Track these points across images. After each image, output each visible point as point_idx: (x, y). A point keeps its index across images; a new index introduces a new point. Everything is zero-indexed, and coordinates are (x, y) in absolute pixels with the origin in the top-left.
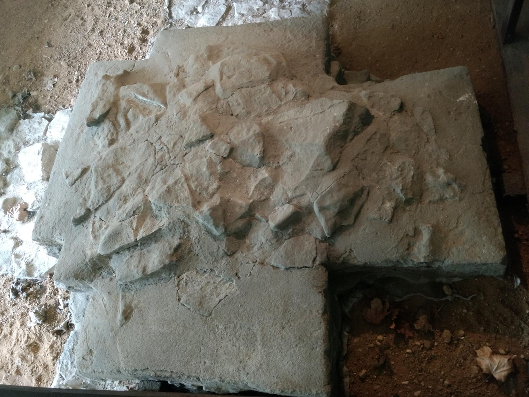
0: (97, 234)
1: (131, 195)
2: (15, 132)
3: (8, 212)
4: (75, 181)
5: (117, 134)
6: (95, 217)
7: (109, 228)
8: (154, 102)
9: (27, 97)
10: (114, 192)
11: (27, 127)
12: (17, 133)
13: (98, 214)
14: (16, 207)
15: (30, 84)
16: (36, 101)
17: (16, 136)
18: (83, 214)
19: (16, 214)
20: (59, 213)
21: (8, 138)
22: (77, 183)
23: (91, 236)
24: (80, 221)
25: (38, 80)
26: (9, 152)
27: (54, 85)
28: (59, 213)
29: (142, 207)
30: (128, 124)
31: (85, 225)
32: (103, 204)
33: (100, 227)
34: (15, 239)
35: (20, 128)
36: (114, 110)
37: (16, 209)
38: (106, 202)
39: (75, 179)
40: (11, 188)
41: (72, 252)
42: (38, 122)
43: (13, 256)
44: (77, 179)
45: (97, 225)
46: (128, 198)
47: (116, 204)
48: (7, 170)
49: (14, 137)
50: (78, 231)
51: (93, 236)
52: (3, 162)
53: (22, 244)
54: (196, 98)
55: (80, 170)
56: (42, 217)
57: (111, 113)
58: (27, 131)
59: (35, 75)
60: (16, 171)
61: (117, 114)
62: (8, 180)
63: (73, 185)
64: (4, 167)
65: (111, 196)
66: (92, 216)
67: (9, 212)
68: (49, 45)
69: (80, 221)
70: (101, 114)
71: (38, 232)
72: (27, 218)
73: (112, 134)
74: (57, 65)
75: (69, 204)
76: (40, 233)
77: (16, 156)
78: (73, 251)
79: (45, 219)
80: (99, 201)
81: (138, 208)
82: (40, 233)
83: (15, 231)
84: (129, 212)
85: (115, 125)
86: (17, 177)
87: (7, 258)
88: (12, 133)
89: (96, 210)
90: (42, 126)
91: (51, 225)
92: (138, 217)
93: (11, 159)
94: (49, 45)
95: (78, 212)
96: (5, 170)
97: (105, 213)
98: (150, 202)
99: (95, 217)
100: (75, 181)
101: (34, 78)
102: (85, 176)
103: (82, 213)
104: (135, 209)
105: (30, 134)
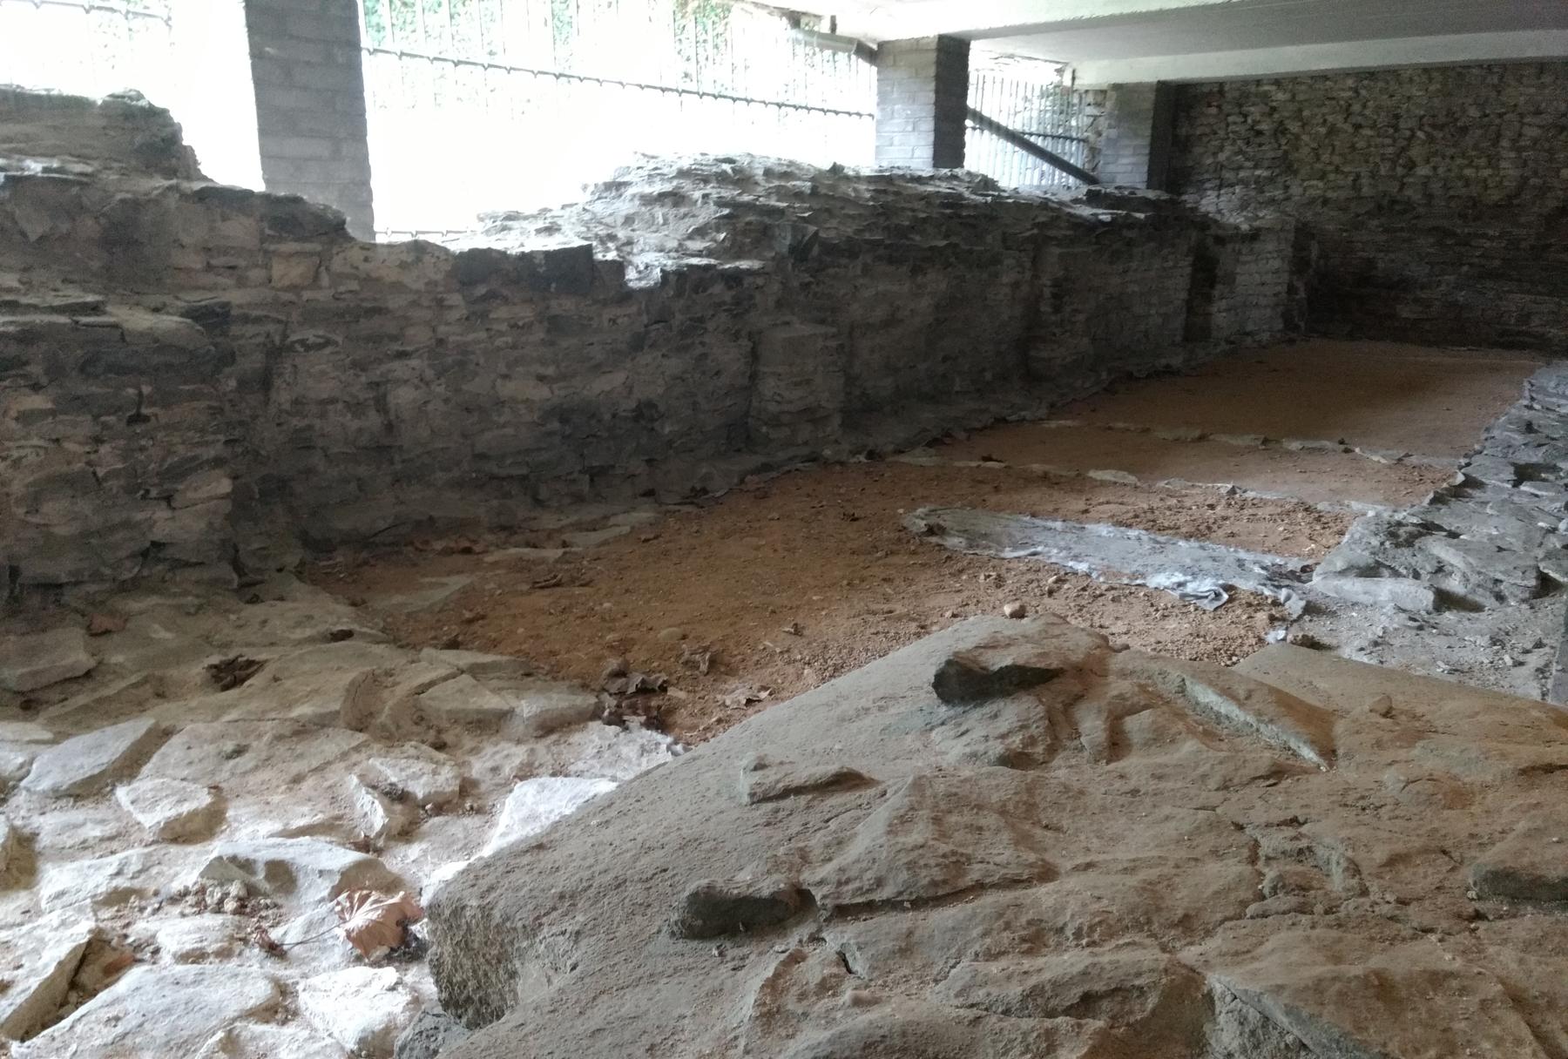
0: (791, 1004)
1: (1078, 934)
2: (554, 737)
3: (345, 895)
4: (786, 793)
5: (1052, 750)
6: (816, 939)
7: (874, 1014)
8: (1268, 731)
9: (653, 691)
10: (980, 887)
11: (597, 741)
12: (556, 743)
13: (837, 937)
14: (383, 897)
15: (680, 671)
16: (671, 711)
17: (548, 747)
18: (766, 893)
19: (362, 917)
20: (636, 859)
21: (519, 742)
22: (788, 803)
23: (751, 999)
24: (724, 919)
25: (711, 678)
26: (495, 770)
27: (749, 702)
28: (636, 859)
29: (1152, 1001)
30: (1116, 745)
31: (730, 953)
32: (892, 905)
33: (826, 987)
34: (283, 990)
35: (576, 738)
36: (1071, 685)
37: (375, 902)
38: (918, 904)
39: (796, 783)
40: (414, 850)
41: (583, 1026)
42: (642, 746)
43: (220, 1034)
44: (799, 791)
45: (814, 968)
46: (1052, 940)
47: (975, 933)
48: (449, 802)
49: (541, 747)
50: (677, 962)
51: (759, 1004)
52: (455, 777)
53: (284, 1022)
54: (1533, 768)
55: (833, 768)
56: (540, 847)
57: (1056, 685)
58: (591, 751)
59: (713, 663)
60: (471, 822)
61: (1079, 698)
62: (426, 827)
63: (766, 799)
64: (448, 789)
65: (957, 895)
66: (805, 931)
67: (350, 898)
68: (798, 631)
69: (724, 919)
70: (1021, 662)
71: (483, 884)
72: (384, 950)
73: (1032, 741)
74: (790, 670)
75: (706, 846)
76: (491, 889)
77: (506, 787)
78: (593, 1024)
79: (547, 859)
80: (879, 883)
81: (1118, 992)
82: (491, 889)
83: (306, 969)
84: (1057, 985)
85: (1059, 729)
86: (461, 836)
87: (186, 1033)
88: (541, 737)
89: (843, 912)
90: (644, 760)
91: (561, 883)
92: (1103, 1034)
93: (483, 788)
94: (798, 631)
95: (745, 876)
96: (440, 800)
97: (887, 945)
98: (1209, 998)
99: (816, 939)
100: (786, 793)
101: (704, 667)
102: (837, 800)
103: (766, 888)
104: (1099, 987)
105: (594, 762)
